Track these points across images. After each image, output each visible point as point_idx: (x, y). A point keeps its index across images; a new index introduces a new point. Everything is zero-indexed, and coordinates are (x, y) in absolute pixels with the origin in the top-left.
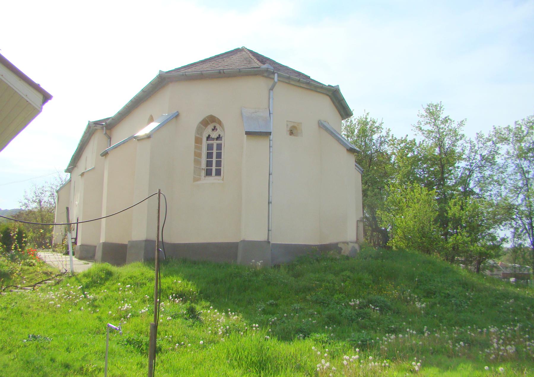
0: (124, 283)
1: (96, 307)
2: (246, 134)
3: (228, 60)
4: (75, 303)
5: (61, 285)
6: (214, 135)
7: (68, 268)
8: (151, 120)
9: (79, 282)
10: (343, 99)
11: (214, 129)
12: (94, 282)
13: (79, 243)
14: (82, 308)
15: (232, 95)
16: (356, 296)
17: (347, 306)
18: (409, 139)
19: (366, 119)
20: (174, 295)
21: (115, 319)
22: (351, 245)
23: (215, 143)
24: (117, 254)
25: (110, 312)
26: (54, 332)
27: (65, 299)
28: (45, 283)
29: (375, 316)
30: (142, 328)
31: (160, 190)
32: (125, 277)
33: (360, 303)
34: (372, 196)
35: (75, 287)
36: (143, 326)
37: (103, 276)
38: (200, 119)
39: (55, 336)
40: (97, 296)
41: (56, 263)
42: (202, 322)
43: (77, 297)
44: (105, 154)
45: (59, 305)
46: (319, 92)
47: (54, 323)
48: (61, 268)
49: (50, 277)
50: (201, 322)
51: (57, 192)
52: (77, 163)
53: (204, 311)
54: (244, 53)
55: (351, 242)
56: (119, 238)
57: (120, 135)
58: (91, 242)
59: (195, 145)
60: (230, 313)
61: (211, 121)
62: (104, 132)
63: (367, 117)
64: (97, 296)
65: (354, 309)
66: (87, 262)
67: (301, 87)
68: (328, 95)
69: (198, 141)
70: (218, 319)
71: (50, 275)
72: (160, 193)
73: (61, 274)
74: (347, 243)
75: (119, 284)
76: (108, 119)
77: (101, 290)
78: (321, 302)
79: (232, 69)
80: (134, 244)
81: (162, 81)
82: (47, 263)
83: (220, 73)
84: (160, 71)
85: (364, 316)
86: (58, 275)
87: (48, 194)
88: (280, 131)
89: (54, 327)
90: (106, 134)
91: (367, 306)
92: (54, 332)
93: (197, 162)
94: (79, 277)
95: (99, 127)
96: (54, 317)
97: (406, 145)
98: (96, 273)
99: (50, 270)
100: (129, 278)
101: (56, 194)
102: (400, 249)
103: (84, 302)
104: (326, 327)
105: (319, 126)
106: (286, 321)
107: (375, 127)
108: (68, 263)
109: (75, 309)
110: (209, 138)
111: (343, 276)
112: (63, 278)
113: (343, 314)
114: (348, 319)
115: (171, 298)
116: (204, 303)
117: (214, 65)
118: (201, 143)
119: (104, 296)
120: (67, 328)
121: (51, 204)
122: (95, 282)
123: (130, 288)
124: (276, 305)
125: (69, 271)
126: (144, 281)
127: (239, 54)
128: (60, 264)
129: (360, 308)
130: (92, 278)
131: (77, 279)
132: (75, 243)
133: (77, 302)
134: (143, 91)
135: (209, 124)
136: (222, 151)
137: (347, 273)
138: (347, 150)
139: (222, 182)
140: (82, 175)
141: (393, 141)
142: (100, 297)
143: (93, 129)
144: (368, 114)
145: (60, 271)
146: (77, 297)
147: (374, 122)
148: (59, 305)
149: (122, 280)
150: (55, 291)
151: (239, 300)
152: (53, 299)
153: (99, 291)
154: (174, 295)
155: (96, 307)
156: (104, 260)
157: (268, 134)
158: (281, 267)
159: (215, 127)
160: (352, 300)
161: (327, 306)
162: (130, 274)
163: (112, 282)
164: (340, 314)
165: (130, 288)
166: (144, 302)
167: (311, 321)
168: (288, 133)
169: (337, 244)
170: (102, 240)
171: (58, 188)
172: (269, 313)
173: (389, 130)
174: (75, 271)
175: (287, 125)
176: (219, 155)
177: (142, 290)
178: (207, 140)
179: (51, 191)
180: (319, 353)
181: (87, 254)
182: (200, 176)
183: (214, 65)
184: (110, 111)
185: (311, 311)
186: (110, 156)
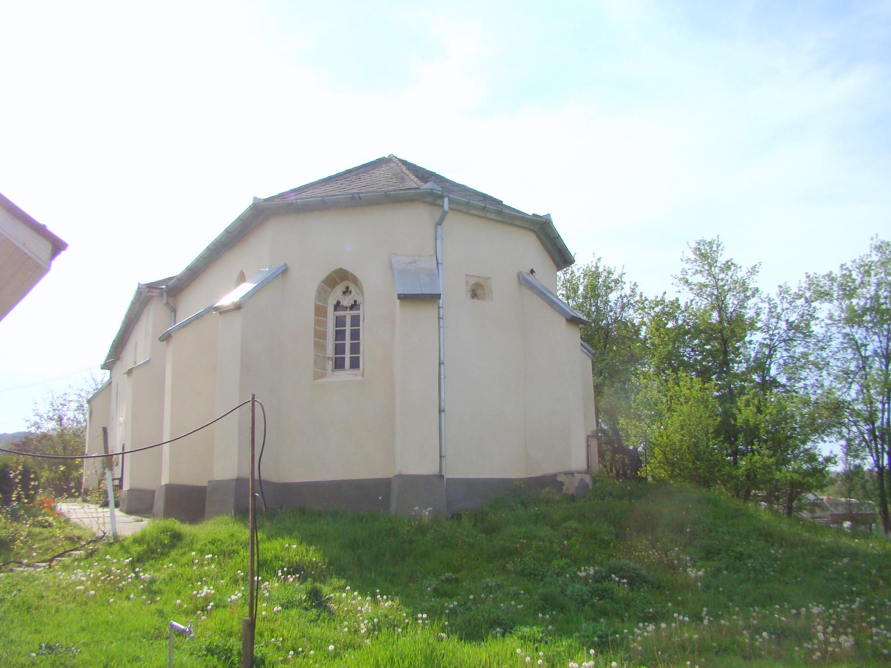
0: (202, 552)
3: (366, 177)
4: (119, 588)
6: (347, 302)
7: (108, 529)
8: (242, 279)
11: (347, 291)
12: (151, 551)
13: (126, 487)
14: (132, 596)
15: (387, 230)
16: (589, 560)
17: (574, 578)
18: (669, 298)
19: (597, 267)
22: (578, 477)
23: (348, 314)
24: (188, 502)
26: (84, 638)
27: (103, 581)
28: (69, 556)
30: (232, 627)
31: (253, 396)
32: (203, 542)
33: (596, 573)
35: (119, 560)
37: (166, 542)
38: (323, 276)
39: (86, 644)
40: (157, 575)
42: (333, 614)
44: (167, 338)
45: (92, 592)
47: (83, 623)
48: (95, 529)
49: (78, 546)
50: (331, 613)
51: (89, 402)
52: (121, 353)
54: (393, 165)
56: (192, 477)
57: (191, 305)
58: (145, 483)
60: (379, 596)
62: (165, 301)
64: (157, 575)
66: (140, 518)
69: (320, 311)
70: (359, 608)
72: (253, 401)
73: (97, 540)
74: (572, 474)
75: (194, 553)
77: (162, 565)
80: (218, 486)
83: (353, 198)
84: (255, 198)
85: (604, 594)
86: (91, 542)
87: (74, 405)
88: (454, 290)
89: (83, 629)
90: (167, 304)
91: (607, 577)
92: (84, 638)
93: (319, 346)
94: (126, 543)
95: (156, 292)
97: (663, 308)
98: (155, 536)
99: (77, 533)
100: (210, 542)
101: (86, 405)
103: (135, 585)
104: (540, 615)
105: (520, 283)
106: (473, 607)
108: (108, 520)
110: (338, 306)
112: (99, 545)
115: (280, 574)
116: (335, 581)
117: (343, 186)
118: (326, 316)
119: (169, 575)
122: (153, 551)
123: (212, 560)
124: (456, 580)
125: (110, 533)
126: (235, 547)
130: (149, 544)
131: (122, 547)
133: (124, 586)
134: (227, 231)
136: (361, 328)
139: (360, 378)
140: (130, 372)
142: (162, 575)
143: (148, 296)
144: (599, 259)
145: (94, 534)
146: (123, 578)
147: (610, 273)
148: (92, 592)
150: (85, 568)
151: (394, 575)
152: (81, 583)
153: (159, 566)
156: (167, 514)
159: (347, 288)
161: (541, 580)
162: (210, 538)
163: (181, 551)
164: (563, 591)
166: (236, 582)
168: (469, 294)
169: (555, 475)
170: (165, 481)
173: (635, 285)
174: (119, 533)
175: (467, 282)
176: (355, 335)
177: (231, 563)
178: (335, 310)
179: (79, 401)
181: (138, 504)
182: (325, 369)
185: (515, 588)
186: (174, 341)
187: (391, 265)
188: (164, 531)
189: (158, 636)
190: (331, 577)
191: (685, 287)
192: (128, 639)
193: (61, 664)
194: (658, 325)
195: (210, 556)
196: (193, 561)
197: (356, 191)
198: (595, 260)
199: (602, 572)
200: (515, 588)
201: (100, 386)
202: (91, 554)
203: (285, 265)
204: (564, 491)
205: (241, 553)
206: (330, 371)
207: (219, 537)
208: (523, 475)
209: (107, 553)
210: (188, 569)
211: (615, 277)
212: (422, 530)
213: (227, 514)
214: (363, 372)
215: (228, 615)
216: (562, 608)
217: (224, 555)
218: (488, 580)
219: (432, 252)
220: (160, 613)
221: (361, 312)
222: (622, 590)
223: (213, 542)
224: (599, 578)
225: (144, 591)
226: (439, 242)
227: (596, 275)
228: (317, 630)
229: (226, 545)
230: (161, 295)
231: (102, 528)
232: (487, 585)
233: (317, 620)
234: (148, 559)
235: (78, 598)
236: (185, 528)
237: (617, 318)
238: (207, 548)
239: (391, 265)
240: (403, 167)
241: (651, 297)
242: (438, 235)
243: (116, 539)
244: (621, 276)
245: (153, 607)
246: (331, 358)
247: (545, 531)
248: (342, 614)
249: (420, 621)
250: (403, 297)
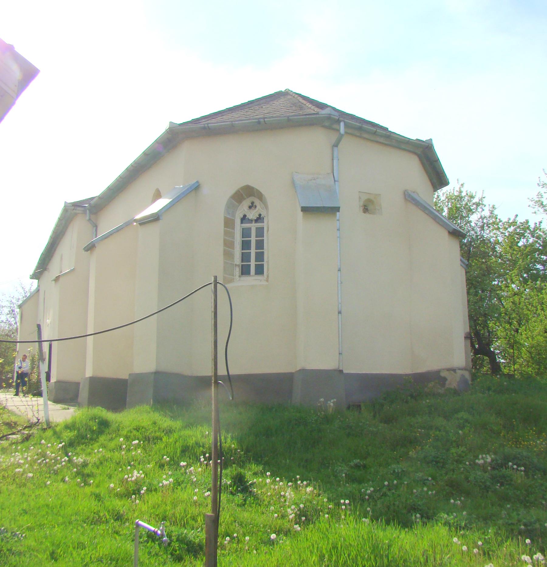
0: (127, 438)
1: (88, 475)
2: (302, 211)
3: (267, 106)
4: (54, 470)
5: (32, 441)
6: (252, 215)
7: (42, 416)
8: (158, 195)
9: (59, 437)
10: (437, 160)
11: (252, 206)
12: (82, 436)
13: (53, 380)
14: (67, 479)
15: (274, 160)
16: (483, 449)
17: (474, 465)
18: (521, 220)
19: (461, 192)
20: (207, 455)
21: (120, 496)
22: (459, 372)
23: (253, 226)
24: (112, 393)
25: (112, 485)
26: (26, 521)
27: (40, 464)
28: (7, 439)
29: (519, 481)
30: (165, 511)
31: (216, 278)
32: (129, 429)
33: (492, 460)
34: (476, 303)
35: (53, 444)
36: (168, 508)
37: (95, 428)
38: (232, 191)
39: (29, 529)
40: (88, 458)
41: (23, 409)
42: (258, 499)
43: (58, 460)
44: (90, 248)
45: (31, 475)
46: (404, 150)
47: (25, 506)
48: (30, 415)
49: (14, 430)
50: (256, 498)
51: (20, 307)
52: (47, 265)
53: (257, 480)
54: (289, 97)
55: (459, 369)
56: (112, 371)
57: (110, 221)
58: (72, 376)
59: (224, 231)
60: (299, 482)
61: (247, 194)
62: (88, 218)
63: (462, 189)
64: (88, 458)
65: (485, 471)
66: (66, 407)
67: (377, 142)
68: (415, 153)
69: (229, 223)
70: (282, 493)
71: (14, 427)
72: (216, 283)
73: (31, 426)
74: (454, 370)
75: (122, 439)
76: (93, 198)
77: (92, 449)
78: (433, 461)
79: (276, 117)
80: (138, 378)
81: (176, 138)
82: (10, 408)
83: (259, 123)
84: (171, 123)
85: (503, 480)
86: (26, 427)
87: (6, 310)
88: (350, 206)
89: (25, 512)
90: (90, 219)
91: (504, 465)
92: (26, 521)
93: (228, 255)
94: (58, 429)
95: (79, 210)
96: (24, 494)
97: (515, 230)
98: (84, 422)
99: (13, 419)
100: (134, 429)
101: (18, 310)
102: (529, 377)
103: (68, 468)
104: (452, 501)
106: (389, 493)
107: (474, 204)
108: (41, 408)
109: (56, 481)
110: (244, 219)
111: (458, 419)
112: (34, 431)
113: (471, 478)
114: (480, 486)
115: (202, 459)
116: (254, 467)
117: (248, 113)
118: (233, 228)
119: (99, 459)
120: (47, 513)
121: (11, 325)
122: (83, 437)
123: (137, 446)
124: (365, 466)
125: (43, 420)
126: (158, 434)
127: (282, 100)
128: (29, 410)
129: (493, 468)
130: (79, 430)
131: (55, 433)
132: (48, 378)
133: (58, 469)
134: (145, 154)
135: (245, 199)
136: (265, 238)
137: (463, 415)
138: (449, 232)
139: (265, 283)
140: (57, 279)
141: (498, 224)
142: (92, 459)
143: (72, 212)
144: (462, 185)
145: (29, 421)
146: (56, 461)
147: (472, 197)
148: (31, 475)
149: (125, 433)
150: (22, 452)
151: (306, 461)
152: (19, 465)
153: (89, 450)
154: (207, 455)
155: (88, 475)
156: (93, 402)
157: (334, 210)
158: (363, 408)
159: (253, 203)
160: (480, 456)
161: (443, 467)
162: (134, 425)
163: (109, 437)
164: (467, 478)
165: (137, 446)
166: (162, 466)
167: (427, 492)
168: (362, 209)
169: (438, 372)
170: (89, 373)
171: (20, 302)
172: (360, 481)
173: (493, 207)
174: (51, 419)
175: (360, 198)
176: (260, 245)
177: (156, 448)
178: (242, 223)
179: (10, 307)
180: (465, 548)
181: (65, 394)
182: (233, 275)
183: (248, 113)
184: (95, 189)
185: (420, 474)
186: (98, 251)
187: (293, 183)
188: (93, 418)
189: (97, 521)
190: (250, 462)
191: (540, 209)
192: (70, 523)
193: (8, 550)
194: (512, 242)
195: (137, 442)
196: (121, 447)
197: (262, 116)
198: (459, 186)
199: (497, 460)
200: (420, 474)
201: (28, 294)
202: (27, 438)
203: (198, 182)
204: (447, 386)
205: (164, 439)
206: (237, 277)
207: (144, 424)
208: (409, 371)
209: (41, 438)
210: (116, 453)
211: (476, 200)
212: (328, 420)
213: (147, 405)
214: (268, 276)
215: (160, 499)
216: (468, 494)
217: (149, 441)
218: (394, 466)
219: (330, 171)
220: (98, 497)
221: (265, 225)
222: (519, 476)
223: (137, 429)
224: (496, 466)
225: (78, 473)
226: (335, 161)
227: (460, 198)
228: (246, 515)
229: (149, 432)
230: (84, 212)
231: (36, 415)
232: (394, 471)
233: (244, 505)
234: (79, 444)
235: (17, 480)
236: (110, 416)
237: (477, 236)
238: (132, 435)
239: (293, 183)
240: (299, 98)
241: (504, 220)
242: (335, 156)
243: (49, 425)
244: (481, 200)
245: (88, 490)
246: (238, 265)
247: (440, 421)
248: (267, 500)
249: (343, 507)
250: (305, 210)
